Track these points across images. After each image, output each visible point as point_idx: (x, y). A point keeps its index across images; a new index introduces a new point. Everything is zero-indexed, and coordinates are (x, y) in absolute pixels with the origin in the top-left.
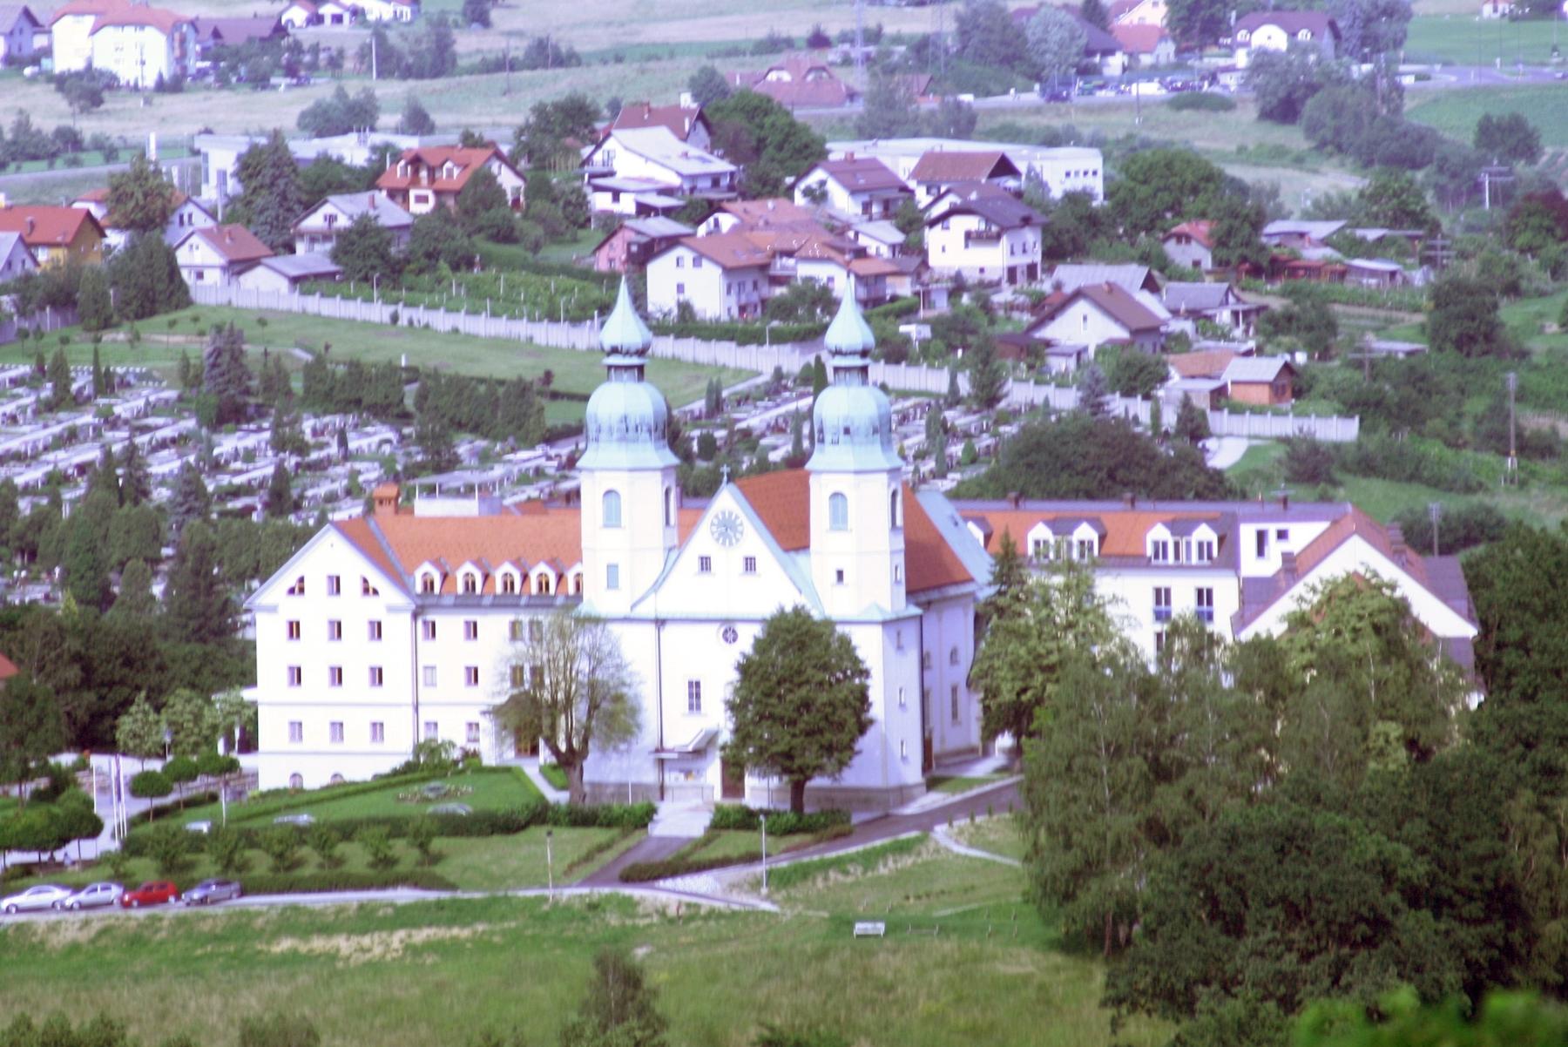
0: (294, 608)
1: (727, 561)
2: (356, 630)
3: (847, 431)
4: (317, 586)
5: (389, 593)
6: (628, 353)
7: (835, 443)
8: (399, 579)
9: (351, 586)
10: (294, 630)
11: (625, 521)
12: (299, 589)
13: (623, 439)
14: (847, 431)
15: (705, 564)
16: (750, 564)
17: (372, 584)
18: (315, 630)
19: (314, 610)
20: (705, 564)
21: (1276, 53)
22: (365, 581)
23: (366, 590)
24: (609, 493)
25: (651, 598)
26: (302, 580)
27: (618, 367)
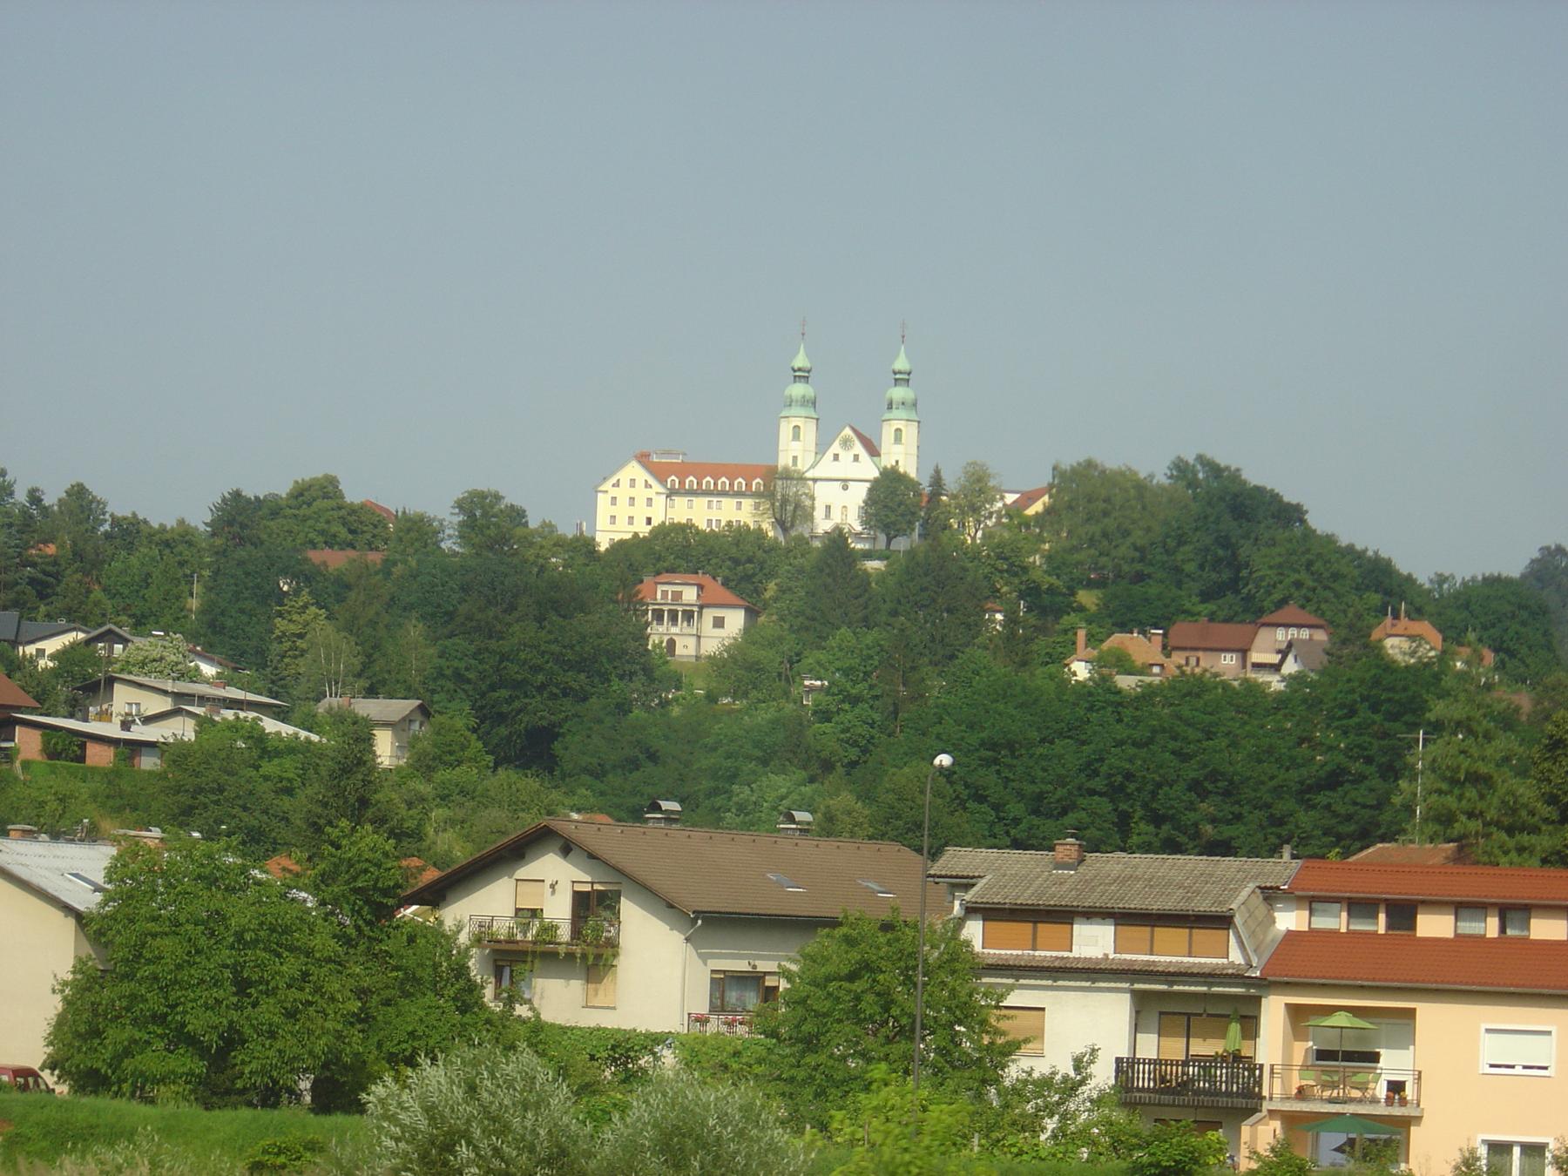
0: (614, 492)
1: (847, 456)
2: (641, 501)
3: (903, 404)
4: (625, 483)
5: (657, 487)
6: (804, 371)
7: (897, 408)
8: (662, 482)
9: (640, 484)
10: (614, 500)
11: (801, 438)
12: (617, 485)
13: (802, 405)
14: (903, 404)
15: (836, 457)
16: (856, 458)
17: (649, 482)
18: (623, 501)
19: (623, 493)
20: (836, 457)
21: (189, 744)
22: (646, 481)
23: (646, 487)
24: (795, 427)
25: (811, 471)
26: (618, 480)
27: (799, 376)
